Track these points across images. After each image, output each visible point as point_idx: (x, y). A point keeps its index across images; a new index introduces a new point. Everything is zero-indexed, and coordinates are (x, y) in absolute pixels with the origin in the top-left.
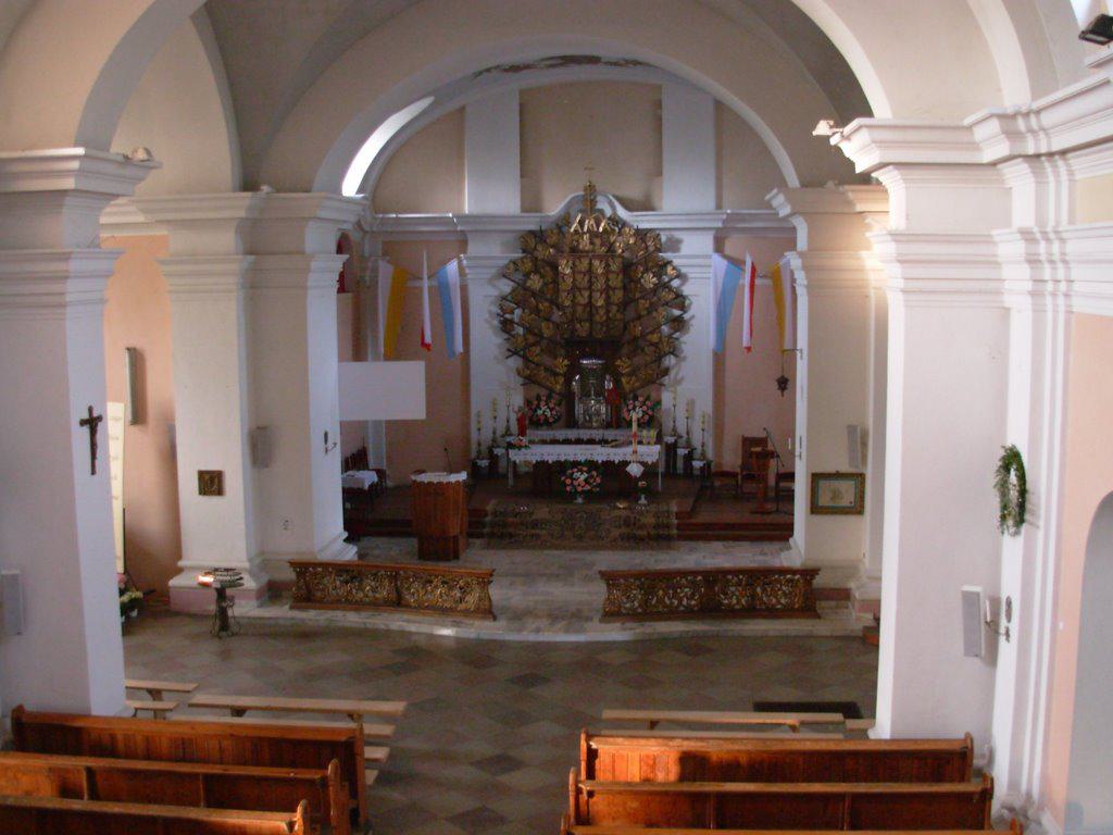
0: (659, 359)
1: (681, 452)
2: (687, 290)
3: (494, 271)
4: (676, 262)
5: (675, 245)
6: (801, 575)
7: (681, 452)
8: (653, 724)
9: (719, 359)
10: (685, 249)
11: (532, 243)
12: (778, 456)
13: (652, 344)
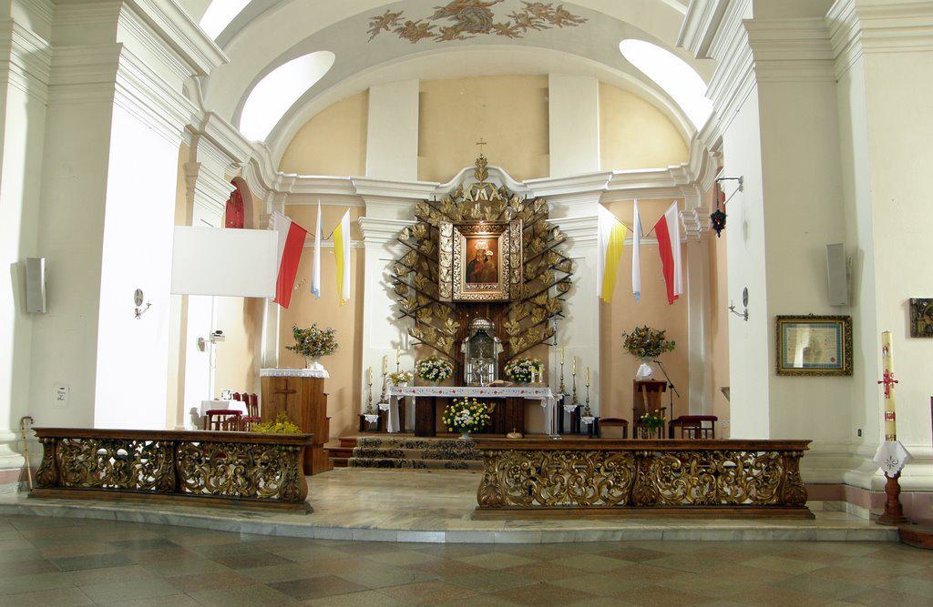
0: (545, 322)
1: (569, 408)
2: (571, 254)
3: (390, 236)
4: (562, 227)
5: (562, 211)
6: (781, 452)
7: (569, 408)
8: (658, 513)
9: (604, 306)
10: (571, 215)
11: (427, 210)
12: (671, 386)
13: (539, 306)
